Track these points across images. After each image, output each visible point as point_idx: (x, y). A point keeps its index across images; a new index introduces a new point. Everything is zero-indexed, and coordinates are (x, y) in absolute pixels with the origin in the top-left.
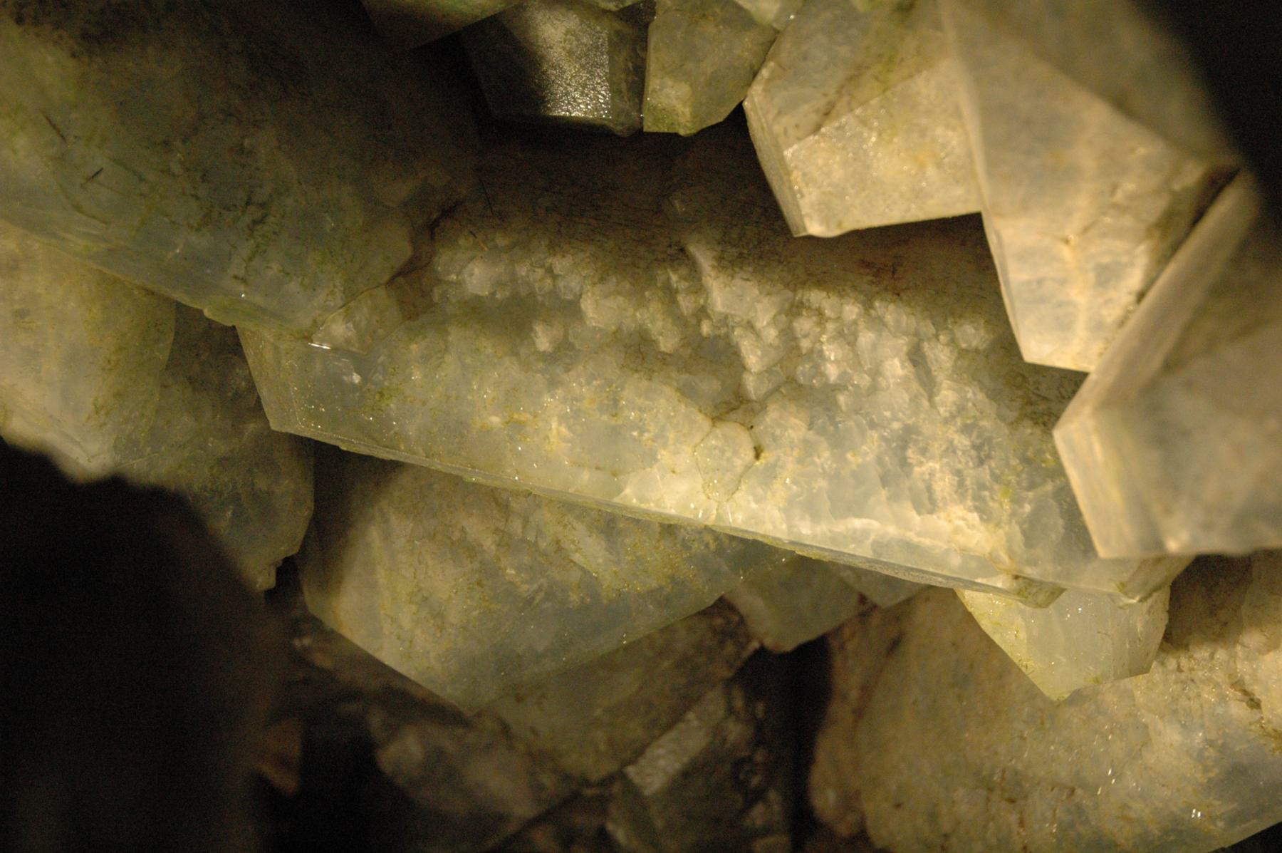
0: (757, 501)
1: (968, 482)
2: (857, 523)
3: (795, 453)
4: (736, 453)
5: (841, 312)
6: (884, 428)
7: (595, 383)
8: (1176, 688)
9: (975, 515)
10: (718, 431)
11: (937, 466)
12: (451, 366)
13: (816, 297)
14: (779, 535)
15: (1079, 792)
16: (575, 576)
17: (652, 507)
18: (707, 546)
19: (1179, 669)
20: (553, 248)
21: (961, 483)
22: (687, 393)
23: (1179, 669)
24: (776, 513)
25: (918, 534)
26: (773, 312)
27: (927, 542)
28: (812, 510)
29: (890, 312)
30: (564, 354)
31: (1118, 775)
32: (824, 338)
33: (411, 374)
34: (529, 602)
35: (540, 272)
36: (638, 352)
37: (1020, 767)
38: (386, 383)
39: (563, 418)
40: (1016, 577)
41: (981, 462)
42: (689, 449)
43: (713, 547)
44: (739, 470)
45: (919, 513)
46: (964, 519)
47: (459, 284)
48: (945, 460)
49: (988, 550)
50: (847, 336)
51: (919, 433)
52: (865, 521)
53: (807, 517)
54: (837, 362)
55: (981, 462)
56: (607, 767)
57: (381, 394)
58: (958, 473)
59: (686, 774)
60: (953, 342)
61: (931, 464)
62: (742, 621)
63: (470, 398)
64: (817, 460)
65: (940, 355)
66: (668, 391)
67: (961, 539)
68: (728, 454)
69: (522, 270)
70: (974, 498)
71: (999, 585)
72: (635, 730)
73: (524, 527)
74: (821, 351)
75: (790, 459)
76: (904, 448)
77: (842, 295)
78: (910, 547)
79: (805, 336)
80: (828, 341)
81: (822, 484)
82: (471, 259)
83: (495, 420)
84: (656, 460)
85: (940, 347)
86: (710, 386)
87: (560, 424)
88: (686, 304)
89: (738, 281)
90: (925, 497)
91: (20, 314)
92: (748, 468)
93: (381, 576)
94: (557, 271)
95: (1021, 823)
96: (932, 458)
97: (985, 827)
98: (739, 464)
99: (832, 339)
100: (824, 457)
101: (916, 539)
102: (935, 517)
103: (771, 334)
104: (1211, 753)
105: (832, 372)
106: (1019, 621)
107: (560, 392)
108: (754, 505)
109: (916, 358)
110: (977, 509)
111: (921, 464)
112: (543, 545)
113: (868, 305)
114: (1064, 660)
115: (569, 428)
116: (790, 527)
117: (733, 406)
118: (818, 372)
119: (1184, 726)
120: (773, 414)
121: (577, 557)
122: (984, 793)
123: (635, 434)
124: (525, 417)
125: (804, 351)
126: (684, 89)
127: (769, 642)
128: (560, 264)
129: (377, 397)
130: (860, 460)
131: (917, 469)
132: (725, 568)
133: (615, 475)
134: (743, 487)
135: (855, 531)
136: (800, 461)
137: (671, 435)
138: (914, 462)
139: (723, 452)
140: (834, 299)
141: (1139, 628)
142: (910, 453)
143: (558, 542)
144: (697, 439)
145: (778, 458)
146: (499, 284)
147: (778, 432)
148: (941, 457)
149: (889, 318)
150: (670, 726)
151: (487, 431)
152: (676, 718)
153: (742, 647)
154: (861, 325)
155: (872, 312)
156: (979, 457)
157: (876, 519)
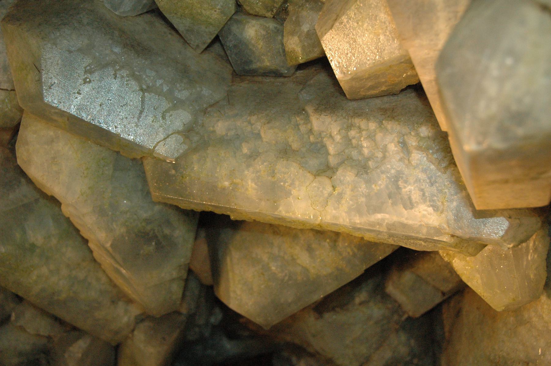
0: (335, 209)
1: (427, 194)
2: (379, 216)
3: (350, 187)
4: (324, 188)
5: (368, 127)
6: (388, 173)
7: (265, 164)
9: (431, 208)
10: (316, 180)
11: (412, 188)
12: (209, 164)
13: (357, 121)
14: (345, 224)
16: (299, 269)
17: (290, 215)
18: (349, 253)
20: (251, 114)
21: (424, 195)
22: (303, 166)
24: (344, 214)
25: (407, 219)
26: (339, 129)
27: (410, 222)
28: (358, 211)
29: (389, 125)
30: (253, 156)
32: (362, 139)
33: (194, 168)
35: (245, 124)
36: (285, 152)
37: (505, 354)
38: (184, 172)
39: (253, 180)
40: (453, 236)
41: (432, 184)
42: (304, 188)
43: (351, 253)
44: (326, 195)
45: (406, 209)
46: (426, 211)
47: (214, 132)
48: (416, 185)
49: (438, 224)
50: (371, 137)
51: (403, 174)
52: (382, 214)
53: (357, 215)
54: (367, 147)
55: (432, 184)
57: (183, 177)
58: (422, 190)
60: (418, 135)
61: (409, 187)
62: (400, 306)
63: (216, 175)
64: (360, 189)
65: (412, 142)
66: (294, 164)
67: (425, 220)
68: (321, 189)
69: (239, 123)
70: (430, 201)
71: (445, 240)
73: (279, 251)
74: (362, 144)
75: (348, 189)
76: (397, 181)
77: (368, 120)
78: (404, 226)
79: (354, 138)
80: (364, 140)
81: (363, 199)
82: (218, 121)
83: (227, 184)
84: (291, 194)
85: (412, 137)
86: (314, 162)
87: (252, 183)
88: (303, 128)
89: (322, 116)
90: (408, 202)
91: (54, 158)
92: (330, 195)
94: (253, 122)
96: (410, 184)
98: (326, 193)
99: (366, 139)
100: (363, 188)
101: (405, 222)
102: (413, 210)
103: (338, 138)
105: (366, 151)
107: (251, 169)
108: (334, 211)
109: (404, 145)
110: (432, 206)
111: (405, 187)
112: (286, 257)
113: (381, 123)
114: (498, 291)
115: (255, 184)
116: (350, 220)
117: (326, 170)
118: (361, 153)
120: (340, 172)
123: (282, 184)
124: (238, 181)
125: (354, 145)
126: (296, 39)
127: (411, 314)
128: (253, 119)
129: (181, 178)
130: (378, 188)
131: (403, 190)
133: (275, 202)
134: (329, 203)
135: (378, 219)
136: (352, 190)
137: (297, 183)
138: (402, 187)
139: (318, 188)
140: (365, 121)
141: (532, 276)
142: (400, 183)
143: (292, 256)
144: (308, 184)
145: (343, 190)
146: (229, 129)
147: (342, 178)
148: (414, 183)
149: (389, 127)
150: (377, 349)
151: (224, 189)
153: (401, 316)
154: (377, 131)
155: (382, 126)
156: (430, 182)
157: (387, 214)
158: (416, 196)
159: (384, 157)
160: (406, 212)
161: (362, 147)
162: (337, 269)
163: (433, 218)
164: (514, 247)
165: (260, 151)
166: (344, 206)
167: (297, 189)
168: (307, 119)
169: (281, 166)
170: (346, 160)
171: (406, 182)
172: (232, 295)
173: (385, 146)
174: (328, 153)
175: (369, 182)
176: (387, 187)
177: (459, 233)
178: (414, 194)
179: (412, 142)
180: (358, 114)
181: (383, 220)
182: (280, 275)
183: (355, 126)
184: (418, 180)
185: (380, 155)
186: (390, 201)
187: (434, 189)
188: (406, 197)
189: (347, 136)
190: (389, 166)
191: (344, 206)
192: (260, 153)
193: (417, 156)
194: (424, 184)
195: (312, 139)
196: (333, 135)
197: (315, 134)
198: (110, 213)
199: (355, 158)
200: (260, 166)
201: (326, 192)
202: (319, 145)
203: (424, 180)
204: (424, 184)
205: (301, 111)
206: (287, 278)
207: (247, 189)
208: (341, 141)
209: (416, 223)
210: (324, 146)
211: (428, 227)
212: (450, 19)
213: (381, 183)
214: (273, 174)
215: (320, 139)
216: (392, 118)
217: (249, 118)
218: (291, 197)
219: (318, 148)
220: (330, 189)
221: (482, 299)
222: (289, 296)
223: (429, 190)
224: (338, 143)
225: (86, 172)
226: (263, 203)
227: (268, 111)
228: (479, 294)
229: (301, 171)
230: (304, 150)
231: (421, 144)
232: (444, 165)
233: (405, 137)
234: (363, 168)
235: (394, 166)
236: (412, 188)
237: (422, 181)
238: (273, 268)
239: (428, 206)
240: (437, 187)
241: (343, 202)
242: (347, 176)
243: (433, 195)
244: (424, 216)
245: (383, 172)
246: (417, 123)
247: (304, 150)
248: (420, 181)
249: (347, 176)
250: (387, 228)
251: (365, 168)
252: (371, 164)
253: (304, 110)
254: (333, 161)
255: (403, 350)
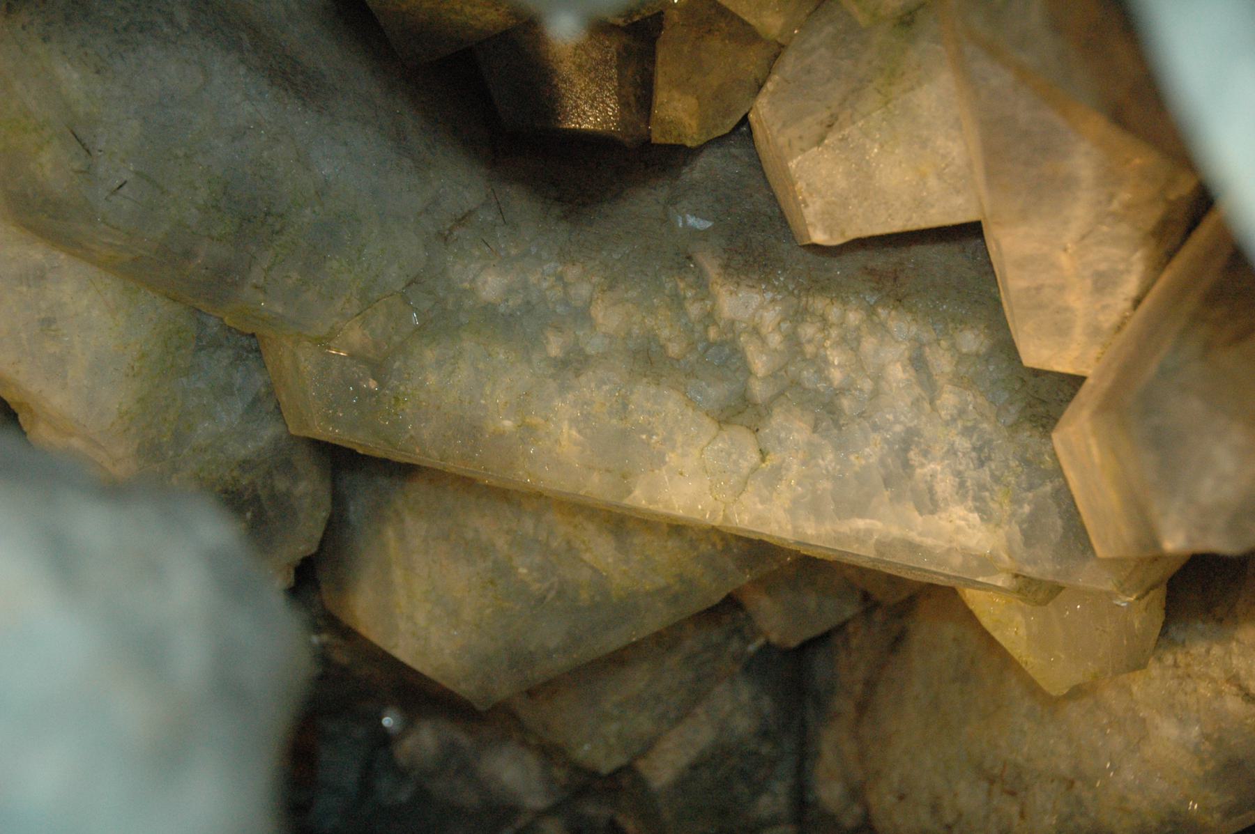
0: (762, 502)
1: (969, 483)
2: (861, 524)
6: (887, 431)
7: (606, 388)
8: (1173, 684)
11: (939, 468)
12: (464, 374)
13: (818, 303)
14: (784, 535)
15: (1078, 784)
16: (586, 574)
18: (714, 545)
19: (1176, 665)
21: (962, 484)
23: (1176, 665)
24: (781, 515)
25: (920, 534)
27: (929, 541)
28: (816, 509)
30: (573, 363)
31: (1116, 769)
33: (425, 379)
34: (542, 599)
36: (648, 360)
37: (1020, 759)
39: (574, 422)
41: (981, 463)
44: (745, 471)
45: (921, 514)
47: (472, 292)
50: (850, 341)
52: (868, 521)
54: (839, 366)
55: (981, 463)
56: (619, 760)
57: (397, 399)
58: (959, 474)
59: (694, 767)
60: (953, 346)
61: (932, 466)
64: (821, 461)
65: (942, 362)
66: (676, 395)
67: (962, 539)
68: (734, 457)
70: (975, 499)
71: (1000, 584)
72: (644, 724)
78: (913, 547)
79: (810, 341)
83: (508, 424)
84: (665, 463)
85: (941, 352)
86: (716, 392)
87: (570, 428)
88: (694, 310)
91: (48, 322)
92: (754, 470)
93: (398, 575)
95: (1022, 815)
97: (987, 817)
98: (745, 466)
100: (828, 459)
101: (918, 539)
102: (936, 517)
103: (775, 340)
104: (1207, 746)
105: (836, 376)
106: (1019, 618)
108: (760, 507)
109: (918, 363)
110: (977, 509)
111: (922, 465)
113: (871, 311)
115: (579, 432)
117: (740, 411)
119: (1181, 720)
120: (778, 418)
121: (587, 557)
122: (985, 785)
123: (644, 437)
124: (536, 420)
127: (774, 638)
128: (572, 273)
130: (863, 462)
131: (918, 471)
132: (731, 566)
134: (750, 488)
135: (858, 531)
136: (804, 463)
137: (680, 438)
139: (729, 455)
142: (912, 454)
143: (569, 542)
146: (510, 291)
147: (783, 435)
148: (943, 459)
149: (893, 325)
150: (679, 720)
151: (501, 435)
152: (684, 714)
155: (875, 318)
156: (979, 458)
157: (879, 520)
158: (945, 485)
159: (876, 393)
160: (920, 519)
161: (826, 360)
162: (680, 577)
163: (980, 535)
164: (1138, 599)
165: (589, 350)
166: (785, 493)
167: (680, 451)
168: (702, 286)
169: (641, 394)
170: (788, 388)
171: (925, 453)
172: (403, 625)
173: (882, 367)
174: (748, 372)
175: (842, 446)
176: (882, 462)
177: (1029, 570)
178: (942, 481)
179: (942, 362)
180: (820, 286)
181: (869, 532)
182: (535, 587)
183: (813, 314)
184: (952, 452)
185: (867, 385)
186: (887, 494)
187: (985, 474)
188: (922, 486)
189: (795, 333)
190: (890, 417)
191: (785, 493)
192: (587, 358)
193: (949, 399)
194: (963, 462)
195: (713, 334)
196: (764, 331)
197: (721, 324)
198: (171, 453)
199: (807, 385)
200: (594, 390)
201: (746, 464)
202: (727, 350)
203: (964, 455)
204: (963, 462)
205: (684, 261)
206: (552, 594)
207: (557, 441)
208: (780, 347)
209: (941, 543)
210: (737, 352)
211: (966, 552)
212: (1100, 202)
213: (870, 453)
214: (623, 409)
215: (730, 336)
216: (899, 301)
217: (560, 269)
218: (664, 469)
219: (723, 356)
220: (756, 457)
221: (1023, 670)
222: (549, 635)
223: (972, 475)
224: (776, 350)
225: (137, 364)
226: (595, 478)
227: (605, 253)
228: (1016, 657)
229: (690, 412)
230: (692, 358)
231: (963, 370)
232: (1010, 420)
233: (927, 350)
234: (826, 410)
235: (902, 418)
236: (939, 468)
237: (960, 454)
238: (523, 571)
239: (971, 511)
240: (991, 471)
241: (782, 487)
242: (792, 429)
243: (982, 487)
244: (959, 530)
245: (876, 428)
246: (953, 320)
247: (692, 358)
248: (955, 454)
249: (792, 429)
250: (877, 551)
251: (834, 413)
252: (846, 403)
253: (689, 258)
254: (759, 390)
255: (743, 725)
